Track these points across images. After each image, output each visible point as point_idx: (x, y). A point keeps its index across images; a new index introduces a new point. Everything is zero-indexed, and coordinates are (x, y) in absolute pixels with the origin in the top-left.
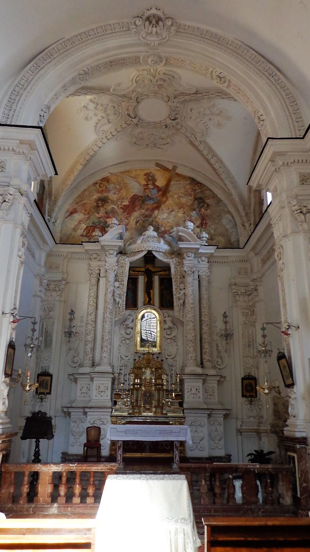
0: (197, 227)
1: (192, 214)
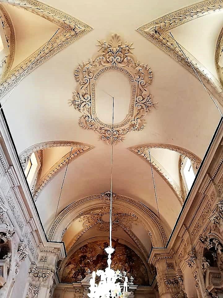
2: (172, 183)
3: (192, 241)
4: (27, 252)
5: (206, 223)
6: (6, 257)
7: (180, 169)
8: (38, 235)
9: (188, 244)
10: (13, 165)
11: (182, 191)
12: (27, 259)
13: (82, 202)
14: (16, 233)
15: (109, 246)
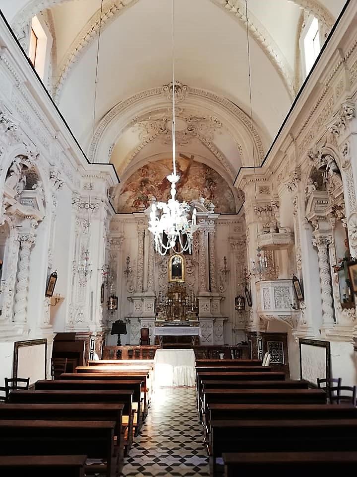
0: (208, 199)
1: (204, 190)
2: (281, 65)
3: (298, 156)
4: (63, 177)
5: (322, 132)
6: (37, 186)
7: (299, 37)
8: (73, 154)
9: (292, 161)
10: (6, 47)
11: (297, 78)
12: (64, 187)
13: (135, 100)
14: (40, 154)
15: (172, 173)
